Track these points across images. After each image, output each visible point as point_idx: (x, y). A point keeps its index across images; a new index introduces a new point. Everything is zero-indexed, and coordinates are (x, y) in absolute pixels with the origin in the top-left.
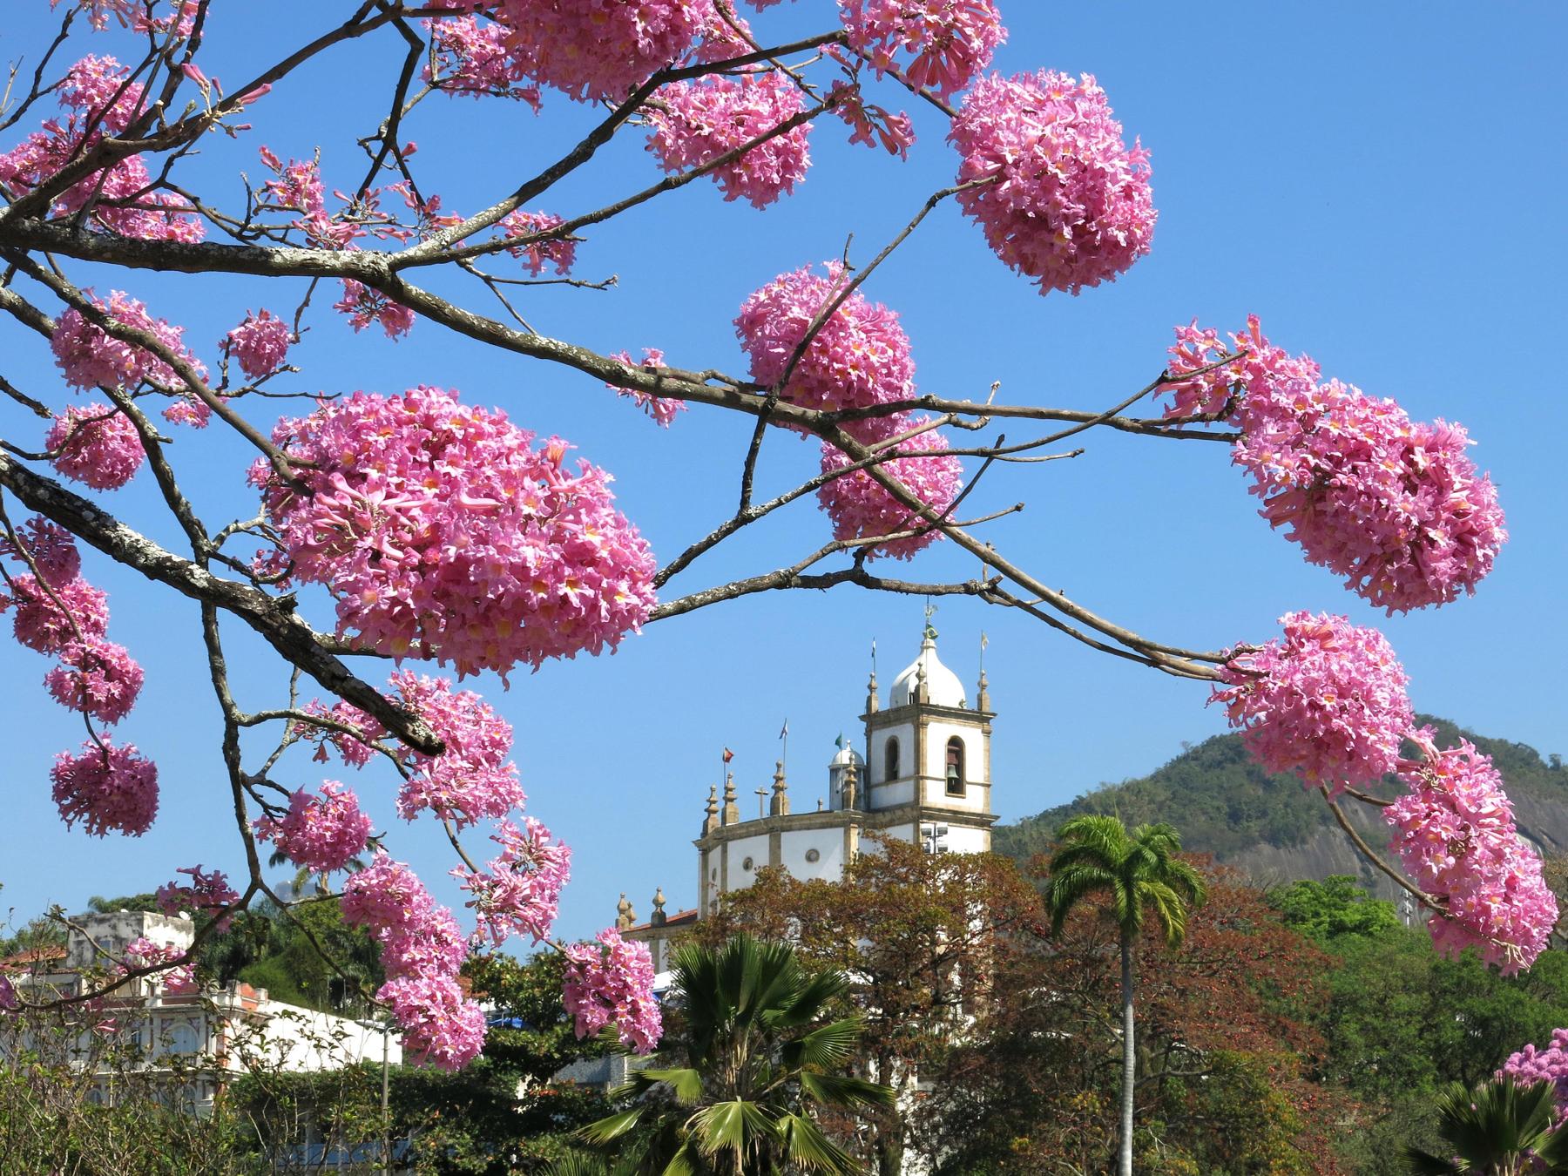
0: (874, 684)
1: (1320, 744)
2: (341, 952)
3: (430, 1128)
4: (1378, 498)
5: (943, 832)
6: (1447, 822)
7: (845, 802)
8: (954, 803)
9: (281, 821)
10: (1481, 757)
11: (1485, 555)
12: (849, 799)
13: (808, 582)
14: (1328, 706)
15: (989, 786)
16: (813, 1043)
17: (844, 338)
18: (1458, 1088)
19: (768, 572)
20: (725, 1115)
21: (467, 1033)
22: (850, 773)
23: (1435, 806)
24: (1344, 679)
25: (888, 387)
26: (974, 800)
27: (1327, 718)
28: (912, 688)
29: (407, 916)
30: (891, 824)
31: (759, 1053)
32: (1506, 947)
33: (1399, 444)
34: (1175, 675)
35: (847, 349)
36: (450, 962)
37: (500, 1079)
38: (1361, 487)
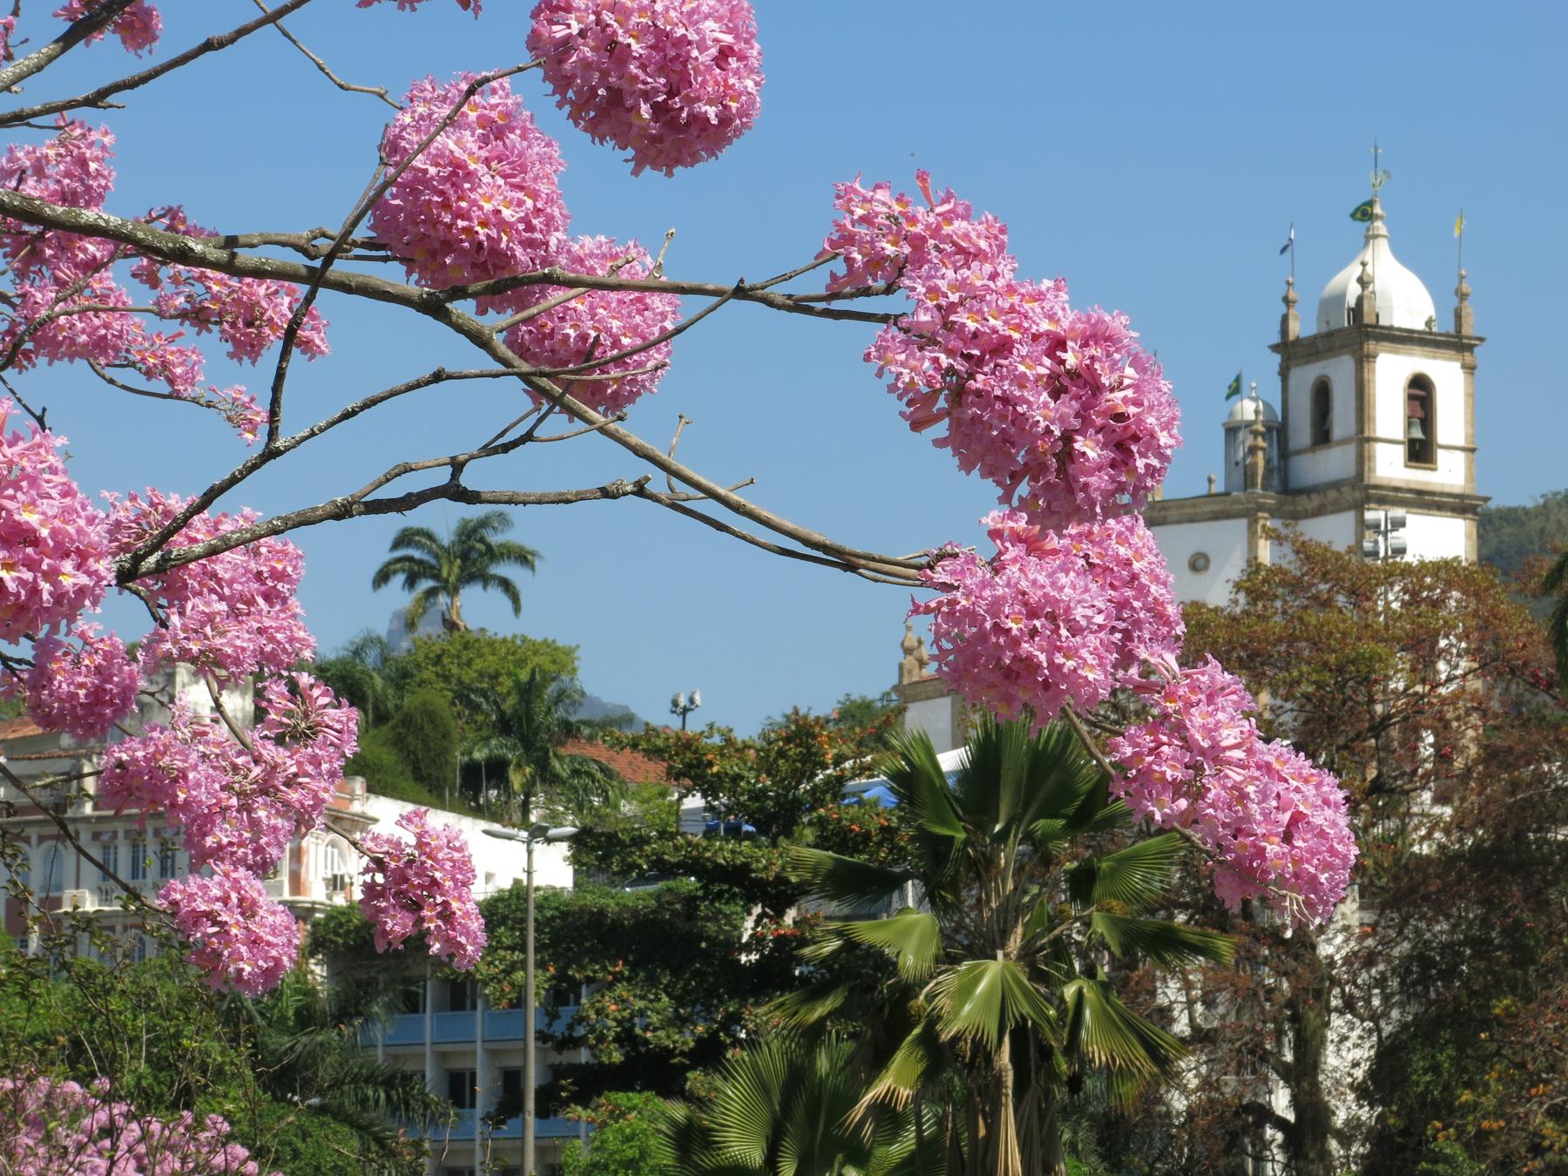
0: (1292, 295)
1: (1009, 674)
2: (480, 718)
3: (610, 986)
5: (1399, 524)
6: (1173, 758)
7: (1248, 479)
9: (25, 676)
10: (1228, 676)
11: (1147, 466)
12: (1254, 475)
13: (495, 451)
14: (1014, 627)
15: (1473, 450)
16: (1113, 872)
17: (471, 190)
19: (321, 503)
20: (976, 981)
21: (269, 944)
22: (1256, 434)
23: (1164, 739)
24: (1035, 596)
25: (529, 244)
26: (1449, 472)
27: (1015, 642)
28: (1351, 301)
29: (182, 796)
30: (1319, 512)
31: (1031, 882)
32: (1284, 897)
33: (1043, 340)
34: (876, 581)
35: (474, 203)
36: (268, 844)
37: (720, 912)
38: (998, 392)
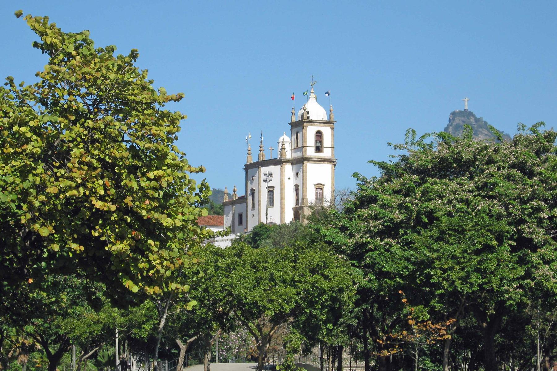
4: (100, 349)
18: (97, 254)
26: (327, 153)
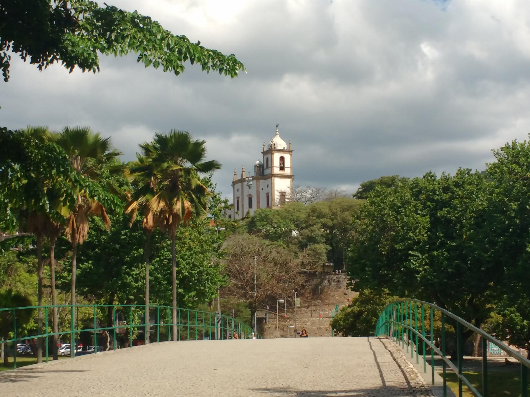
8: (282, 172)
26: (288, 171)
